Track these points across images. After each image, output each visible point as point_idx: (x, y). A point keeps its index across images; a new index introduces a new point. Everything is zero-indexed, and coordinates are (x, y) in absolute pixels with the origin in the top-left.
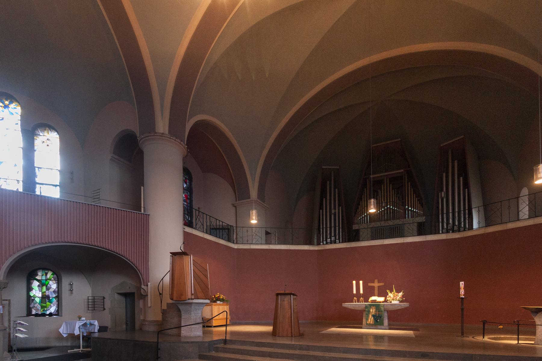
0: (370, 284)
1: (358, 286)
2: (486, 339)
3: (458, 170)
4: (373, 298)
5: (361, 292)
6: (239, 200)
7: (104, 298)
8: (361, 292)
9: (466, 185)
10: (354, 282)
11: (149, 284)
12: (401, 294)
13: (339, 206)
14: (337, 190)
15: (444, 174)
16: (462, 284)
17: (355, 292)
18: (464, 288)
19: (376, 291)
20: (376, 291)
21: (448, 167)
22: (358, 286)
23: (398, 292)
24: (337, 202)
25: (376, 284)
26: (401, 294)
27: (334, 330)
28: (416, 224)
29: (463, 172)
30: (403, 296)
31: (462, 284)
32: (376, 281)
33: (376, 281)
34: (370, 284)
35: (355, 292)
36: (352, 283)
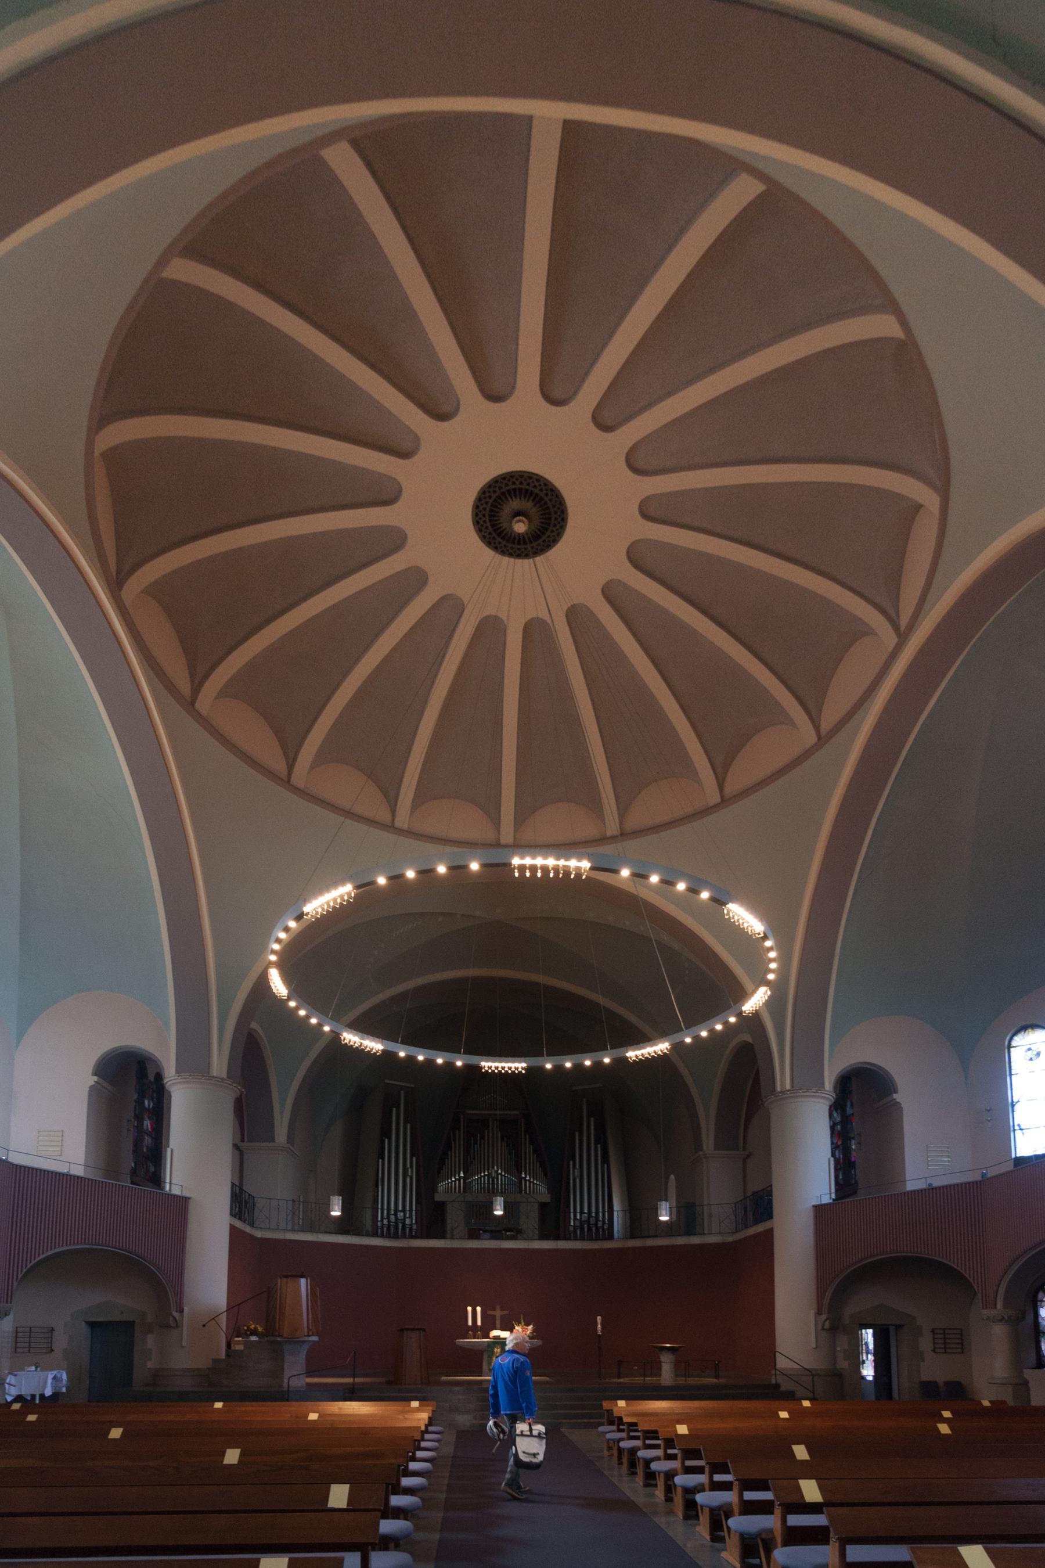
0: (490, 1312)
1: (475, 1314)
2: (622, 1380)
3: (595, 1130)
4: (495, 1333)
5: (479, 1323)
6: (249, 1141)
7: (53, 1330)
8: (479, 1323)
9: (606, 1160)
10: (469, 1309)
11: (186, 1308)
12: (530, 1327)
13: (412, 1156)
14: (409, 1126)
15: (577, 1134)
16: (599, 1318)
17: (470, 1323)
18: (602, 1324)
19: (498, 1322)
20: (498, 1322)
21: (581, 1125)
22: (475, 1314)
23: (527, 1325)
24: (408, 1151)
25: (498, 1313)
26: (530, 1327)
27: (444, 1378)
28: (536, 1206)
29: (601, 1139)
30: (534, 1331)
31: (599, 1318)
32: (498, 1307)
33: (498, 1307)
34: (490, 1312)
35: (470, 1323)
36: (467, 1311)
